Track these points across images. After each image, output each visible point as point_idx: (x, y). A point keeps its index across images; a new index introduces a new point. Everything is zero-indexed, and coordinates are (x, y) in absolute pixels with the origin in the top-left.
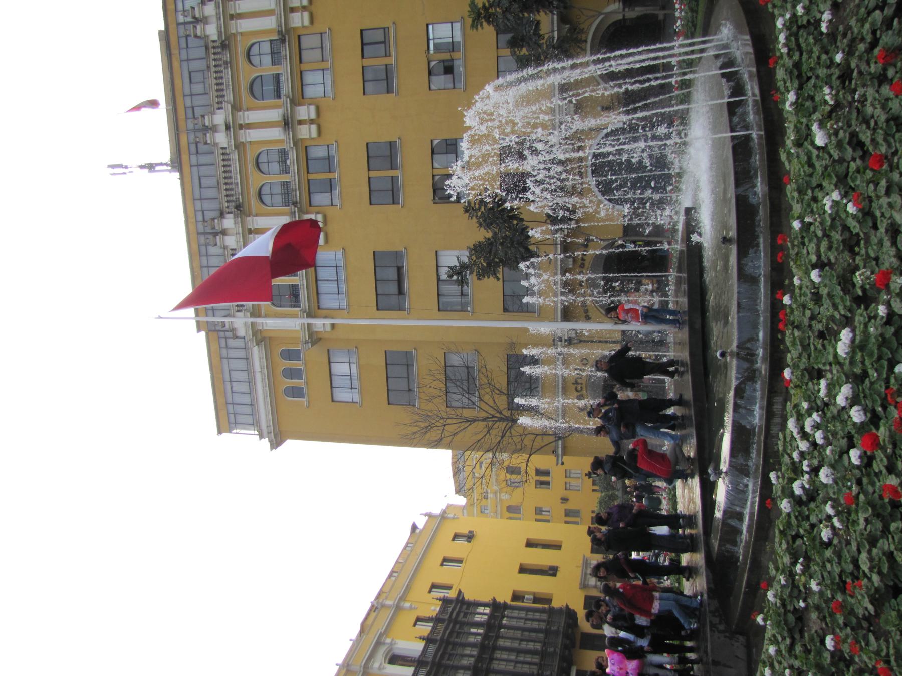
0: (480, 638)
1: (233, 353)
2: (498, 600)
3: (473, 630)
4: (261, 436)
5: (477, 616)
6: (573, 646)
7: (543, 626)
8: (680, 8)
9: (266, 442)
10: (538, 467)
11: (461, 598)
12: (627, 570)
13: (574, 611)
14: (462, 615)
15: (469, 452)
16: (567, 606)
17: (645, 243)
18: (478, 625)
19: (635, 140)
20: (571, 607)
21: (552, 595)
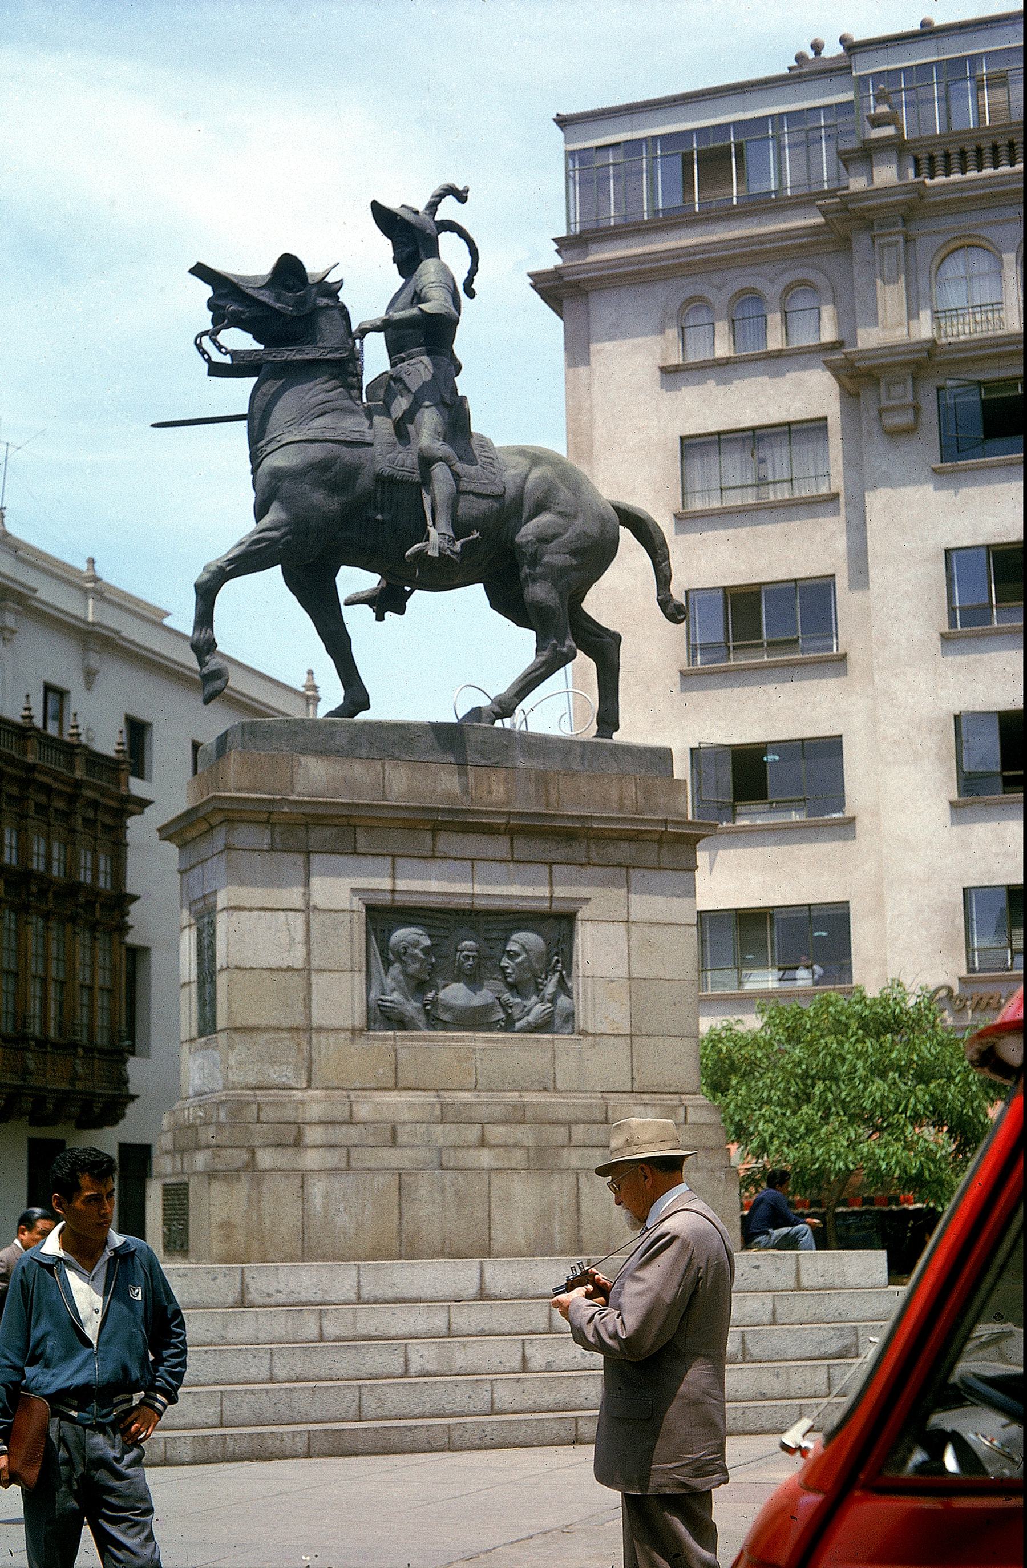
0: (89, 880)
1: (984, 318)
2: (133, 908)
3: (103, 864)
4: (563, 245)
5: (42, 842)
6: (36, 1121)
7: (35, 1029)
8: (748, 1122)
9: (550, 260)
10: (138, 902)
11: (130, 807)
12: (108, 1254)
13: (123, 1116)
14: (43, 799)
15: (453, 760)
16: (133, 1098)
17: (797, 1242)
18: (23, 850)
19: (32, 768)
20: (131, 1109)
21: (148, 1057)
